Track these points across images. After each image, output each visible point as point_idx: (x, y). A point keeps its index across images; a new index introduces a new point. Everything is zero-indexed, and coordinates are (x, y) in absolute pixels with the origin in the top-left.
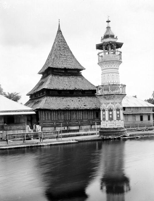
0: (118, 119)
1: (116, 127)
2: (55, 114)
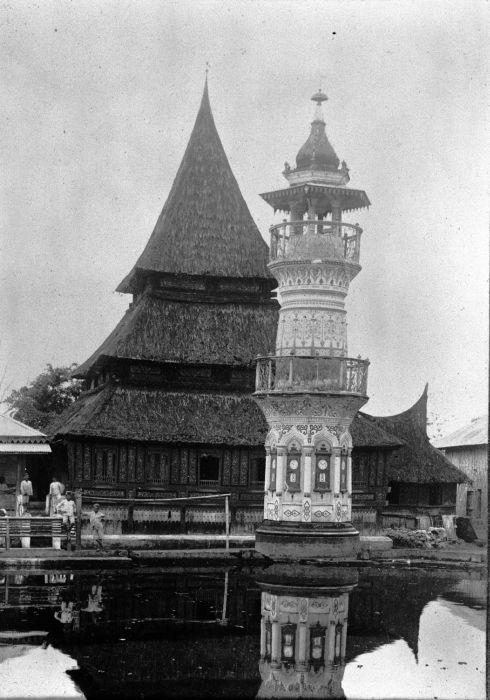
0: (322, 488)
1: (309, 521)
2: (131, 457)
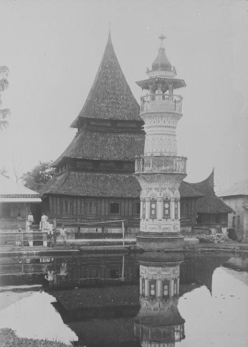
0: (166, 216)
